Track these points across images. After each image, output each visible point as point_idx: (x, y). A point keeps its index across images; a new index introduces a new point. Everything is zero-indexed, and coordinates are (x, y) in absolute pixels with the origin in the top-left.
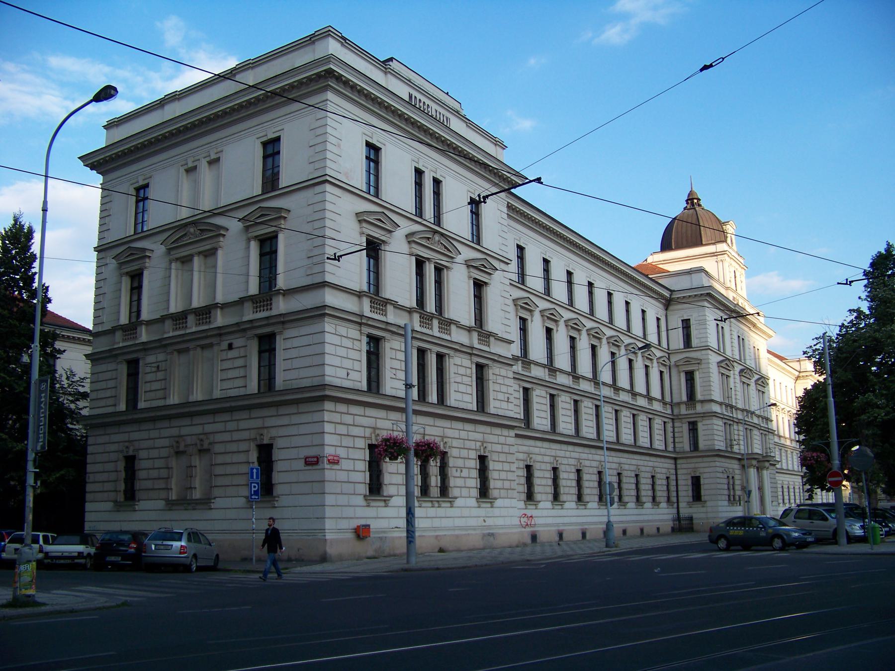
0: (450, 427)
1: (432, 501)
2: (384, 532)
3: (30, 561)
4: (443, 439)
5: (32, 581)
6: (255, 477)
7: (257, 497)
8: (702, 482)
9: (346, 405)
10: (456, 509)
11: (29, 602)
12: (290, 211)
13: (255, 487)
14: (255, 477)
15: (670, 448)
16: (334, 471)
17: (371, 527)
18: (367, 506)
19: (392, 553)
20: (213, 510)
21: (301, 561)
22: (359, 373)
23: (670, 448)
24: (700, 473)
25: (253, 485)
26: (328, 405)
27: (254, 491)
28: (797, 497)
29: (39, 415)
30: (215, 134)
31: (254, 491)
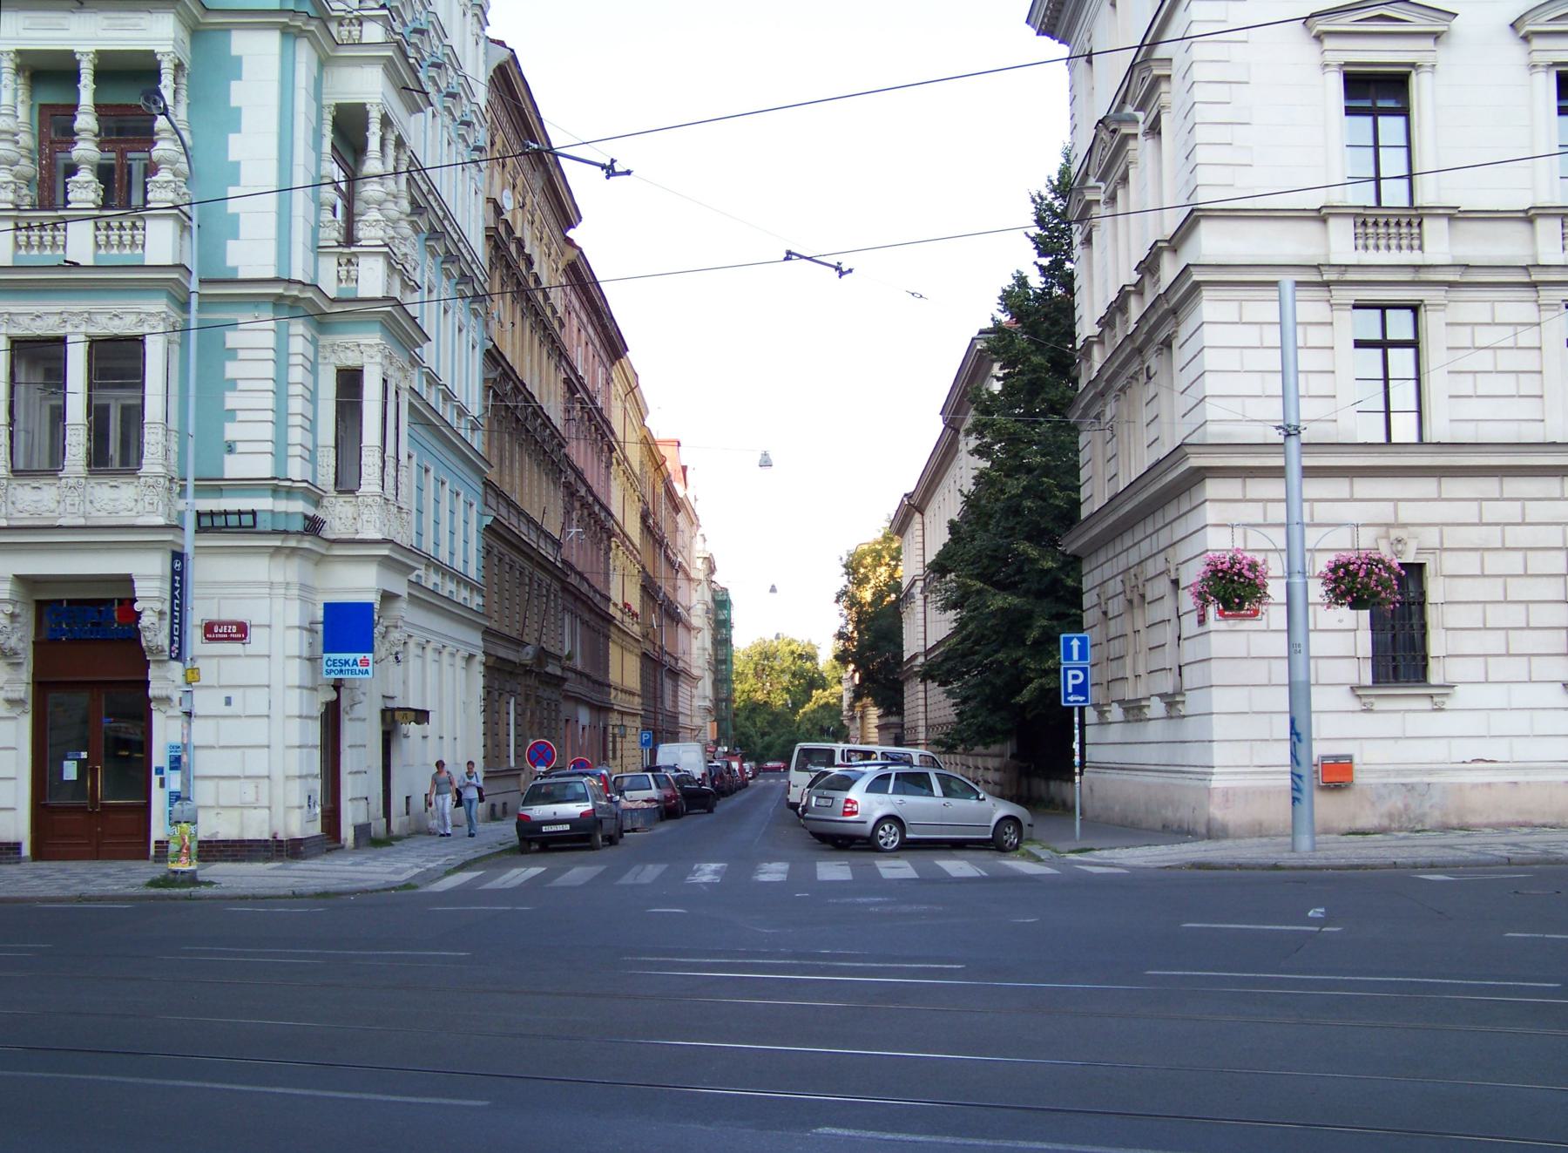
0: (1240, 496)
1: (1431, 696)
2: (1430, 772)
3: (179, 822)
4: (1387, 532)
5: (180, 851)
6: (1076, 656)
7: (1082, 699)
8: (1435, 590)
9: (1239, 481)
10: (1380, 715)
11: (191, 879)
12: (1171, 60)
13: (1075, 677)
14: (1076, 656)
15: (1404, 429)
16: (1243, 635)
17: (1356, 760)
18: (1363, 711)
19: (1454, 821)
20: (1151, 722)
21: (1130, 829)
22: (1537, 376)
23: (1404, 429)
24: (1420, 550)
25: (1070, 673)
26: (1213, 488)
27: (1074, 686)
28: (611, 745)
29: (181, 616)
30: (122, 15)
31: (1074, 686)
